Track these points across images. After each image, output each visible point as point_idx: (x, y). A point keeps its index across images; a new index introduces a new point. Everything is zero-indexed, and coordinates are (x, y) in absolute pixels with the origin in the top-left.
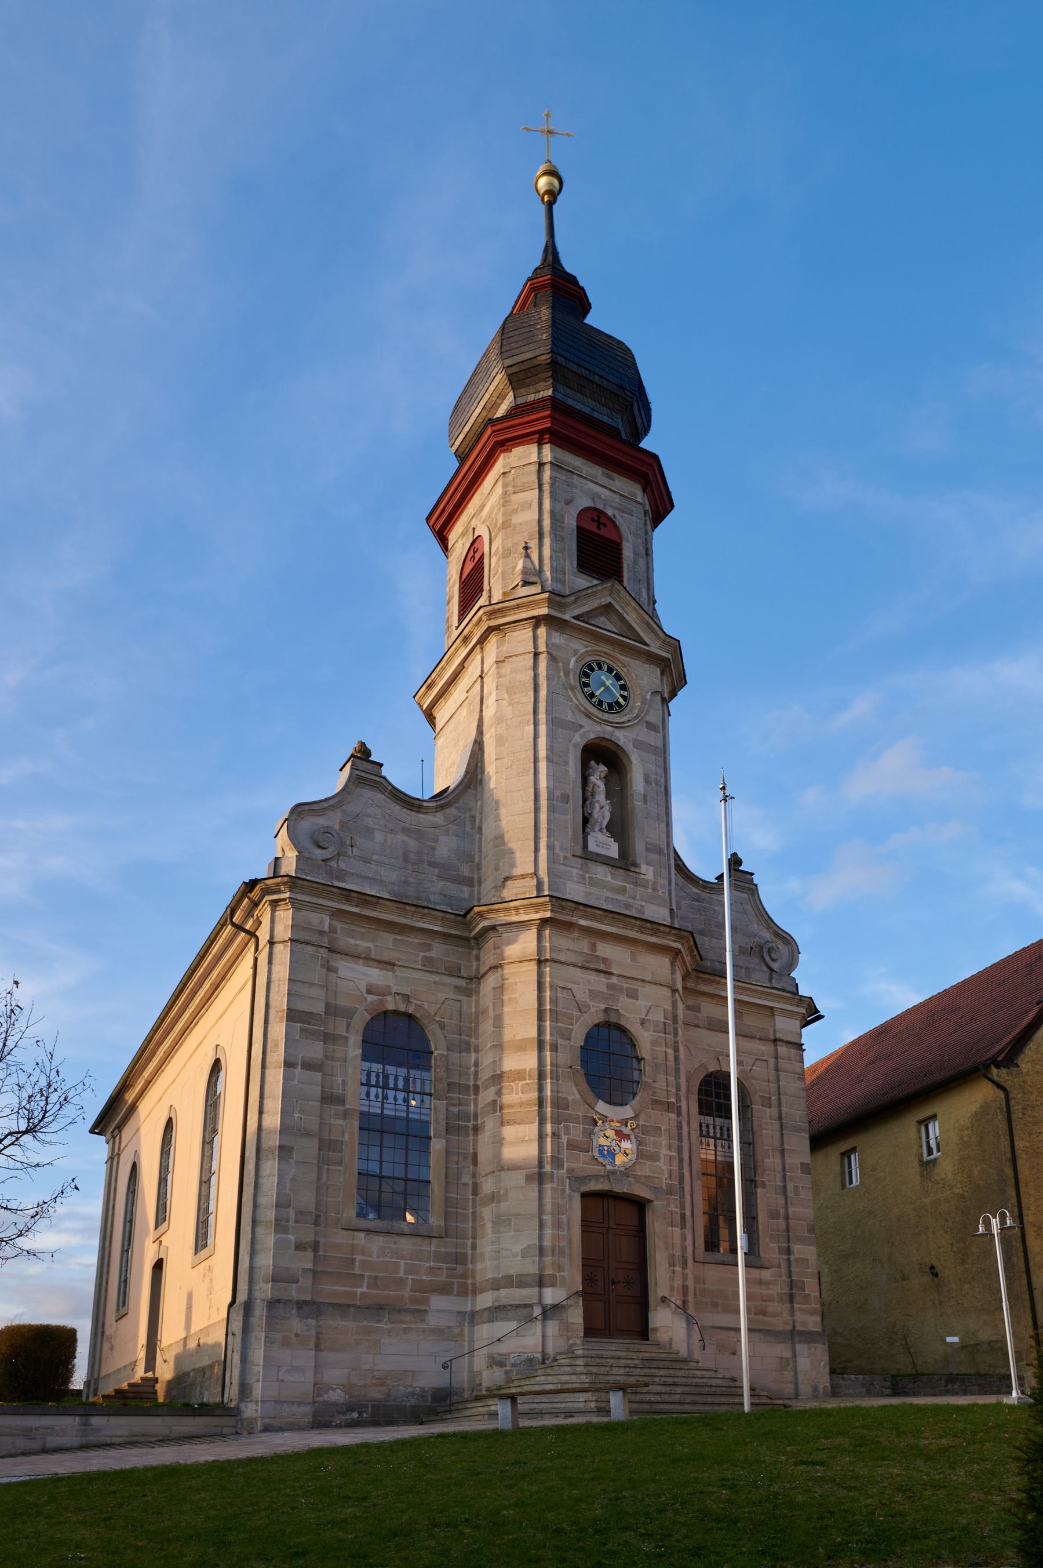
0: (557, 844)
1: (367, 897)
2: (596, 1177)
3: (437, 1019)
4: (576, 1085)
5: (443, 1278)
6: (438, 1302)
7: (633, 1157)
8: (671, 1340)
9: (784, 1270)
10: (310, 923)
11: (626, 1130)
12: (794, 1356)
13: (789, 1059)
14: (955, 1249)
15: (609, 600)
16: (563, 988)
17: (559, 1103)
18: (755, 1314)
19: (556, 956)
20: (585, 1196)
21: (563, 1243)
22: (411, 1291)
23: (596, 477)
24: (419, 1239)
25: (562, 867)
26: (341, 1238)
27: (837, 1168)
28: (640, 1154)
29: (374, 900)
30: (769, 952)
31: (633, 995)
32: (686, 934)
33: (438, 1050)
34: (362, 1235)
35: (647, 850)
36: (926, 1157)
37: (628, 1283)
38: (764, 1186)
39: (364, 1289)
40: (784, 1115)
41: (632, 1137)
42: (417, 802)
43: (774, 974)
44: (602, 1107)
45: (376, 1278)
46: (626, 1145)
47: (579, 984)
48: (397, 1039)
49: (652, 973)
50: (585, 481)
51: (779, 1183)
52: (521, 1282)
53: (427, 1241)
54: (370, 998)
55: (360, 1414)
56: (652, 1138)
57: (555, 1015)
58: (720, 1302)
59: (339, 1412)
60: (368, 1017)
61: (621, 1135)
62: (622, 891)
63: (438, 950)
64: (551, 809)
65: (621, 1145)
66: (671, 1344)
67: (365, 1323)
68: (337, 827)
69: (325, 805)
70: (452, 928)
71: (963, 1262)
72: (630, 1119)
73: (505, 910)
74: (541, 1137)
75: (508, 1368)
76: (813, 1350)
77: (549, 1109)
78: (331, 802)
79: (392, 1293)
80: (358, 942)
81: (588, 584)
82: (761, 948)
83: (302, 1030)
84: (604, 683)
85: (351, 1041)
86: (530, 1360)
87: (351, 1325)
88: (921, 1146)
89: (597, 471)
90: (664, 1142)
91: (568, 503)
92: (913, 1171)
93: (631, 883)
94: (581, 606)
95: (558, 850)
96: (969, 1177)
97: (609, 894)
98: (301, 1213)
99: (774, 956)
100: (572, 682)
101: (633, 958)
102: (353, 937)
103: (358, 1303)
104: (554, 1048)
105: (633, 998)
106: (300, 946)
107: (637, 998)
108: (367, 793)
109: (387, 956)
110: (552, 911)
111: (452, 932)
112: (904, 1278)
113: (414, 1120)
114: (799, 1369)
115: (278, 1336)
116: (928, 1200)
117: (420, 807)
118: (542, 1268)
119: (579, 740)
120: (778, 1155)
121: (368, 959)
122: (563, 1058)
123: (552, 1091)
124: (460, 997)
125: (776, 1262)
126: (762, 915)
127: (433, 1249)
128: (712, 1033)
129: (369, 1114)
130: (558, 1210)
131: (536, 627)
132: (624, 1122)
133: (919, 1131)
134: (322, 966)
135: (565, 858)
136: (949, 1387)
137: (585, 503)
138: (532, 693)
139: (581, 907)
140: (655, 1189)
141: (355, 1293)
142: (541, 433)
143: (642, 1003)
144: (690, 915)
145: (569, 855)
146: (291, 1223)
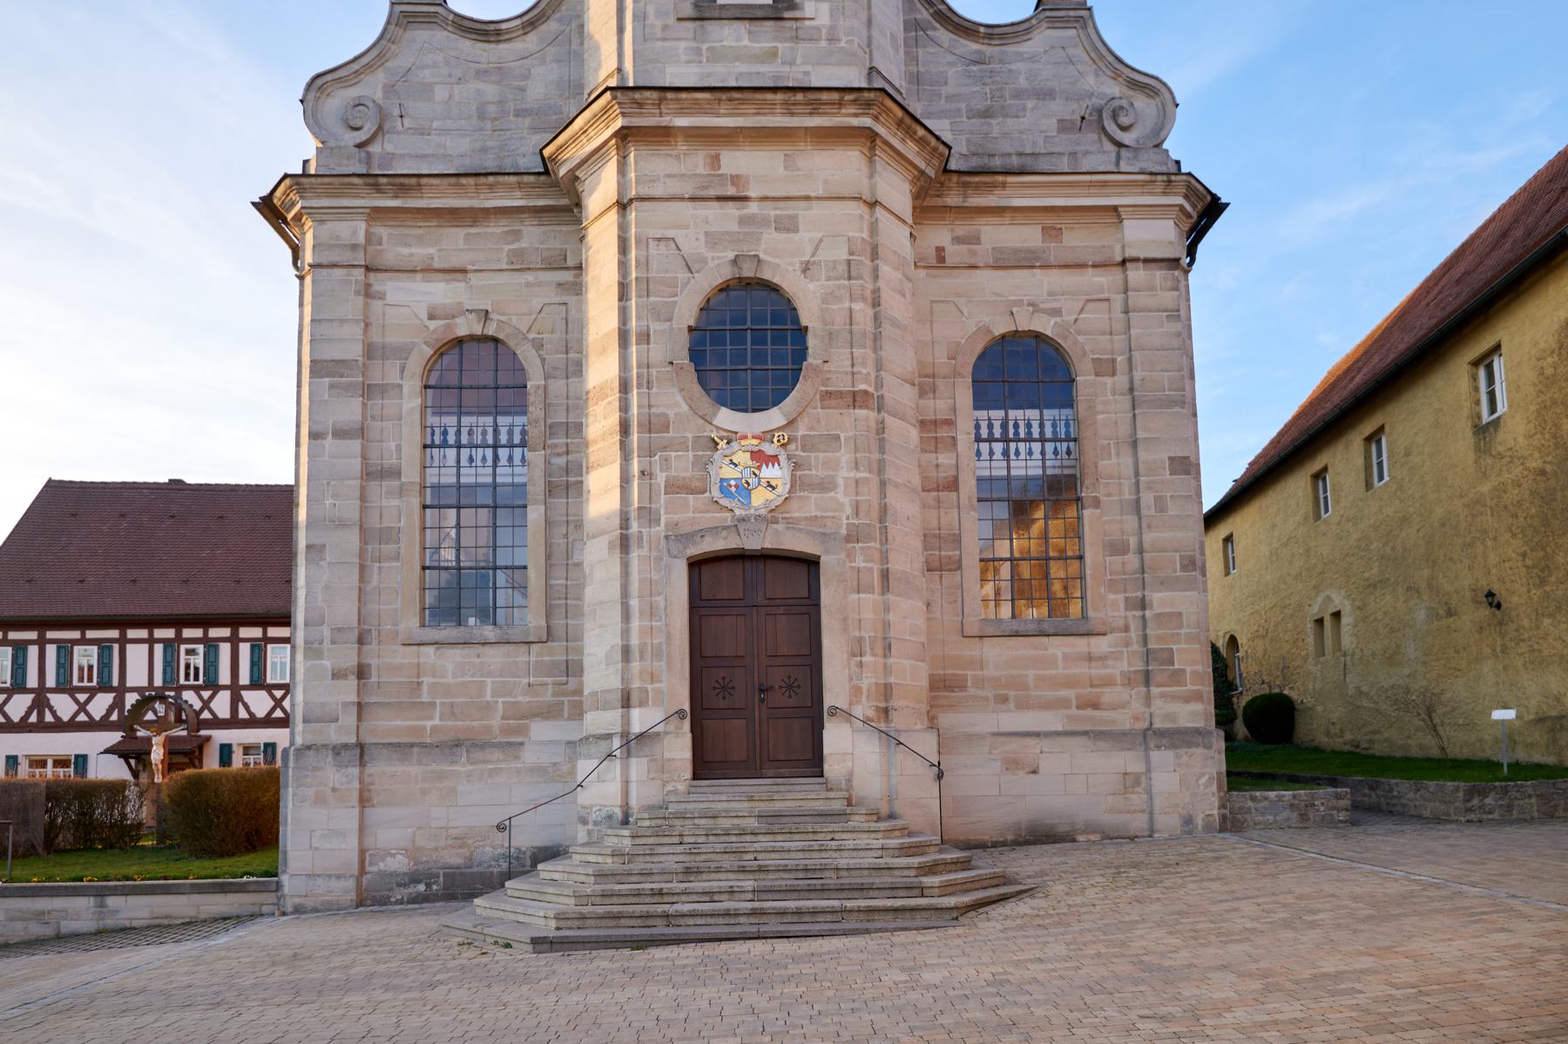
0: (651, 9)
1: (402, 180)
2: (714, 530)
3: (531, 336)
4: (682, 390)
5: (547, 697)
6: (540, 730)
7: (783, 490)
8: (851, 774)
9: (1134, 634)
11: (770, 449)
12: (1149, 770)
13: (1152, 288)
14: (1529, 562)
16: (659, 240)
18: (1078, 708)
19: (646, 191)
22: (503, 718)
24: (511, 648)
25: (659, 44)
26: (403, 656)
27: (1360, 462)
29: (413, 181)
30: (1115, 116)
31: (788, 226)
32: (872, 95)
33: (534, 381)
34: (430, 650)
36: (1486, 417)
37: (790, 687)
38: (1096, 503)
39: (437, 722)
40: (1137, 383)
41: (783, 458)
42: (492, 27)
43: (1124, 153)
44: (727, 418)
45: (452, 705)
47: (687, 227)
48: (479, 374)
49: (825, 181)
51: (1127, 497)
53: (524, 648)
54: (433, 325)
55: (428, 886)
56: (821, 455)
57: (646, 287)
58: (1012, 694)
59: (399, 885)
61: (760, 458)
62: (773, 54)
63: (533, 235)
65: (756, 478)
66: (849, 781)
67: (434, 766)
69: (355, 67)
70: (539, 196)
71: (1543, 582)
72: (778, 429)
73: (574, 139)
74: (625, 480)
75: (590, 827)
76: (1185, 758)
78: (365, 60)
79: (475, 724)
80: (414, 250)
82: (1100, 112)
83: (331, 386)
87: (414, 770)
88: (1478, 403)
90: (845, 456)
92: (1463, 442)
93: (787, 40)
95: (651, 19)
96: (1554, 436)
98: (339, 630)
99: (1124, 120)
102: (406, 245)
103: (429, 740)
104: (645, 337)
105: (788, 230)
106: (324, 272)
107: (796, 230)
108: (421, 35)
109: (455, 262)
110: (623, 114)
111: (542, 202)
112: (1450, 613)
113: (504, 485)
114: (1155, 790)
115: (311, 792)
116: (1485, 488)
117: (498, 33)
120: (1126, 450)
122: (657, 352)
123: (639, 407)
124: (565, 299)
125: (1121, 623)
126: (1102, 57)
127: (533, 658)
128: (1000, 273)
129: (991, 479)
130: (650, 588)
133: (1475, 378)
134: (357, 293)
135: (665, 27)
136: (1475, 801)
139: (670, 95)
140: (824, 537)
141: (423, 728)
143: (805, 236)
144: (963, 90)
145: (671, 21)
146: (326, 645)
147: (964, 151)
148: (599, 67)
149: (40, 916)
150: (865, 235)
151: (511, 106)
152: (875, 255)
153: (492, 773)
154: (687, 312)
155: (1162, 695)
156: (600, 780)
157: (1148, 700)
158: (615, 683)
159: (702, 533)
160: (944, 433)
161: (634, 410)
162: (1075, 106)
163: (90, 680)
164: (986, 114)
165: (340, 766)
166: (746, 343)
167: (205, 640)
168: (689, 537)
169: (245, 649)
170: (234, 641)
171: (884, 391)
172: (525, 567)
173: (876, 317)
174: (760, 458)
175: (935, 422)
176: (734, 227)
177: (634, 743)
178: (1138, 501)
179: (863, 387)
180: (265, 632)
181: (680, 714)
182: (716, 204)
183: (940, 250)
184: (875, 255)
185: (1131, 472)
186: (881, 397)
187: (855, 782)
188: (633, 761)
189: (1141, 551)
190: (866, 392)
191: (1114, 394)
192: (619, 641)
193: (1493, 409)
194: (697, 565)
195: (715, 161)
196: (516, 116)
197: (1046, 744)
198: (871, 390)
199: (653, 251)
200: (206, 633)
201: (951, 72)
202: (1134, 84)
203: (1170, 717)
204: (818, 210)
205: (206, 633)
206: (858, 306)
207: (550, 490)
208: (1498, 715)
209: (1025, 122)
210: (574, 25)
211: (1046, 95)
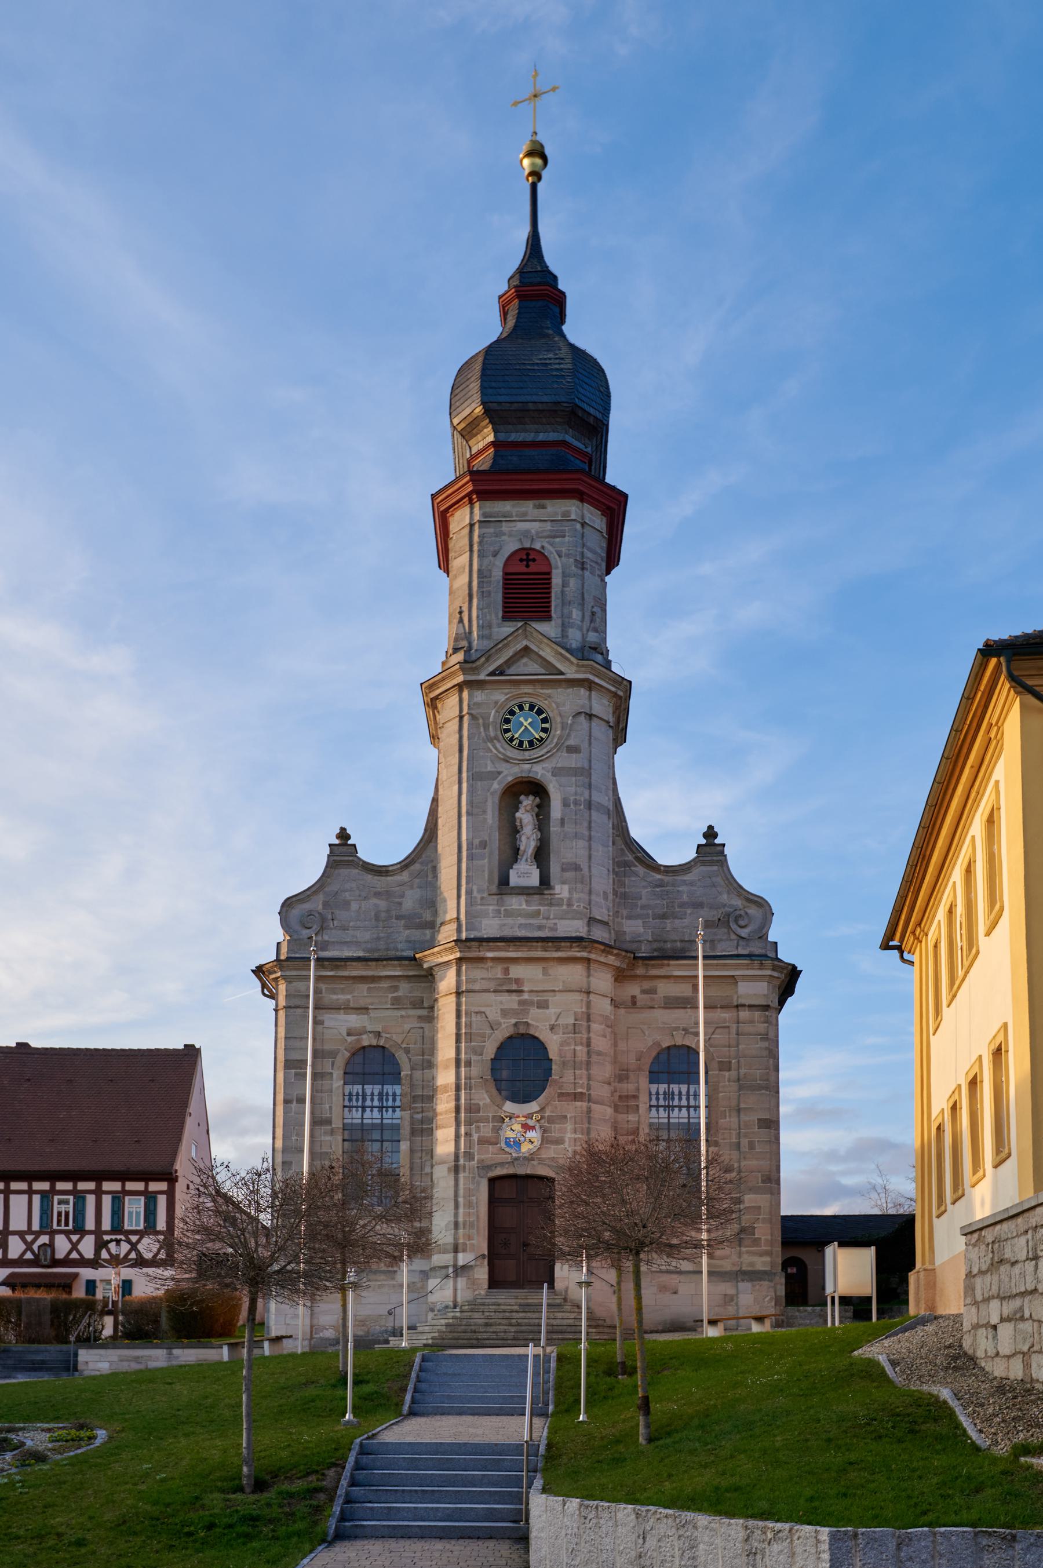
0: (475, 888)
3: (404, 1046)
7: (537, 1143)
10: (299, 991)
11: (531, 1123)
13: (752, 1022)
15: (525, 643)
17: (472, 1109)
19: (471, 987)
21: (473, 1218)
25: (479, 907)
28: (544, 1140)
30: (736, 921)
31: (543, 1005)
35: (563, 870)
41: (537, 1127)
44: (509, 1107)
46: (531, 1134)
48: (373, 1064)
50: (513, 524)
54: (350, 1039)
57: (470, 1037)
59: (331, 1345)
60: (347, 1054)
61: (526, 1127)
62: (537, 913)
63: (404, 989)
64: (470, 857)
69: (308, 893)
73: (433, 954)
77: (463, 1115)
80: (339, 996)
81: (512, 630)
82: (729, 915)
84: (526, 724)
85: (335, 1076)
86: (447, 1307)
89: (528, 506)
90: (569, 1126)
91: (495, 554)
93: (547, 905)
94: (495, 660)
95: (475, 894)
99: (742, 923)
100: (492, 734)
101: (545, 972)
102: (335, 993)
104: (468, 1064)
106: (292, 1010)
107: (547, 1008)
108: (344, 872)
109: (362, 1003)
111: (411, 973)
114: (740, 1304)
117: (387, 871)
118: (456, 1239)
119: (497, 786)
121: (347, 1008)
122: (475, 1071)
130: (469, 1193)
131: (461, 691)
132: (529, 1116)
135: (482, 898)
137: (511, 546)
138: (457, 755)
142: (469, 495)
143: (552, 1011)
145: (485, 895)
147: (650, 939)
148: (445, 912)
149: (137, 1359)
150: (584, 1010)
151: (394, 913)
152: (589, 1020)
153: (380, 1287)
154: (490, 1050)
155: (747, 1252)
156: (441, 1289)
157: (740, 1255)
158: (450, 1239)
159: (496, 1165)
160: (632, 1103)
161: (463, 1101)
162: (715, 912)
163: (67, 1224)
164: (664, 916)
166: (519, 1067)
167: (74, 1192)
168: (489, 1167)
169: (107, 1201)
170: (98, 1193)
171: (591, 1092)
173: (588, 1052)
174: (526, 1127)
175: (627, 1097)
176: (516, 1006)
177: (460, 1270)
178: (739, 1143)
179: (580, 1090)
180: (123, 1186)
181: (483, 1256)
182: (506, 994)
183: (634, 997)
184: (589, 1020)
185: (737, 1126)
186: (589, 1095)
187: (569, 1292)
188: (459, 1279)
189: (740, 1172)
190: (581, 1093)
191: (729, 1081)
192: (452, 1219)
194: (492, 1181)
195: (506, 971)
196: (397, 919)
197: (682, 1278)
198: (584, 1091)
199: (474, 1019)
200: (75, 1186)
201: (644, 892)
202: (749, 900)
203: (752, 1264)
204: (559, 997)
205: (75, 1186)
206: (578, 1048)
207: (413, 1132)
210: (430, 866)
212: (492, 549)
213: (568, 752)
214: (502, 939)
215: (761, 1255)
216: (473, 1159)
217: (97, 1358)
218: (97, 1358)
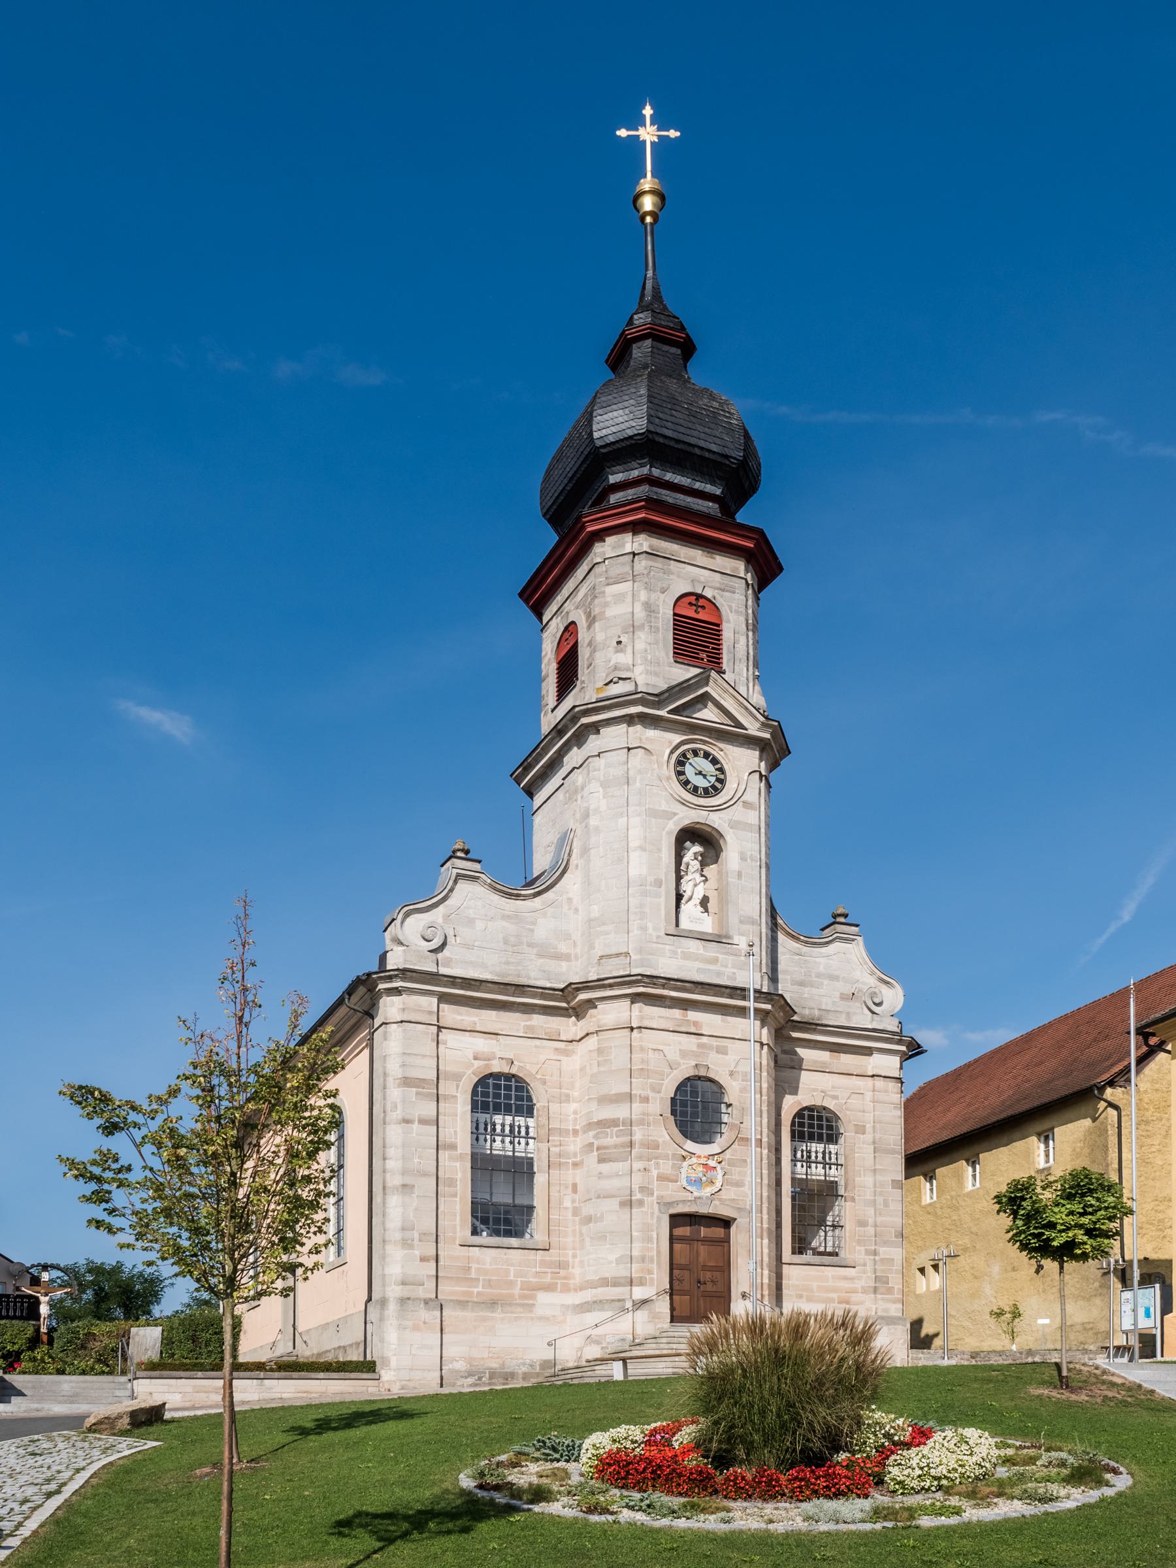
3: (538, 1076)
9: (869, 1268)
11: (712, 1163)
13: (886, 1091)
20: (672, 1216)
23: (695, 558)
31: (722, 1051)
35: (741, 922)
39: (480, 1289)
44: (690, 1145)
52: (616, 1283)
54: (477, 1063)
67: (481, 1314)
68: (440, 920)
83: (417, 1093)
87: (468, 1314)
97: (701, 966)
99: (877, 1001)
107: (726, 1054)
115: (410, 1323)
135: (658, 937)
141: (472, 1293)
143: (731, 1058)
145: (662, 934)
146: (416, 1242)
155: (883, 1299)
159: (677, 1203)
164: (802, 984)
165: (428, 1310)
168: (670, 1204)
172: (726, 1223)
176: (695, 1048)
178: (875, 1201)
193: (1047, 1161)
203: (886, 1310)
208: (1040, 1321)
209: (822, 991)
211: (834, 978)
212: (660, 584)
213: (744, 807)
214: (504, 987)
215: (894, 1302)
216: (652, 1194)
217: (165, 1389)
218: (165, 1389)
